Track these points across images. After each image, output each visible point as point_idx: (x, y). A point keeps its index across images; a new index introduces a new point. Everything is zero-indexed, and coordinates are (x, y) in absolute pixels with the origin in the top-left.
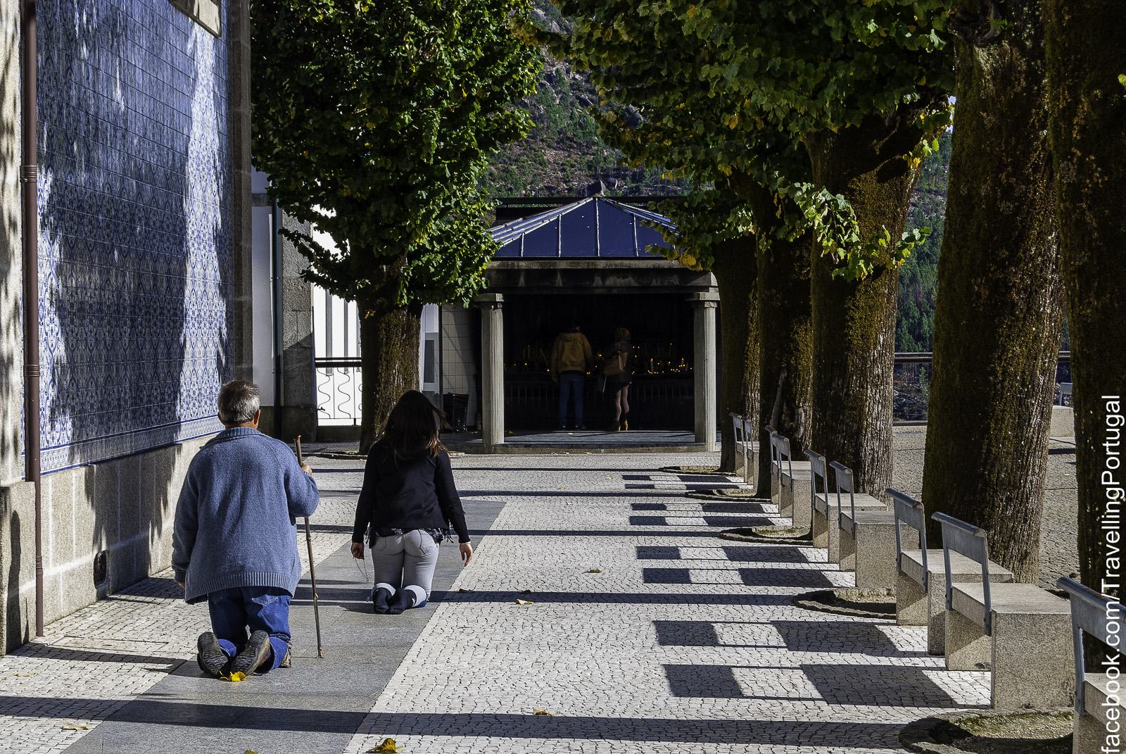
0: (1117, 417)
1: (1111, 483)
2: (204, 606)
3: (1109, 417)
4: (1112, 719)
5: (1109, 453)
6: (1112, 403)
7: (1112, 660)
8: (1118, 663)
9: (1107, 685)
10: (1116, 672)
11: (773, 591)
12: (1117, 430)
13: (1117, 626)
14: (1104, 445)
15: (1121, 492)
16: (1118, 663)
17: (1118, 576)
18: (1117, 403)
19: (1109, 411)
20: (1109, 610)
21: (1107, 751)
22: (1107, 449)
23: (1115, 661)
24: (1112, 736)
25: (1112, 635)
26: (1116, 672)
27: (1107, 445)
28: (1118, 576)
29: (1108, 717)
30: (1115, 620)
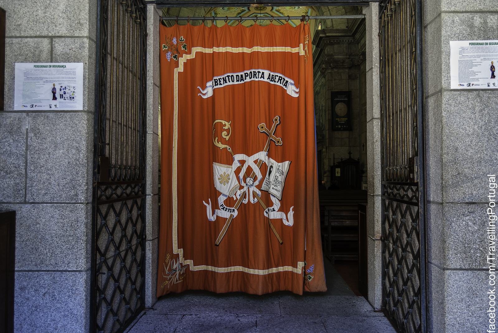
0: (494, 184)
1: (491, 213)
2: (357, 160)
3: (490, 184)
4: (492, 317)
5: (490, 200)
6: (492, 178)
7: (492, 291)
8: (494, 293)
9: (490, 303)
10: (494, 204)
11: (204, 62)
12: (494, 190)
13: (491, 186)
14: (488, 196)
15: (496, 186)
16: (494, 293)
17: (209, 199)
18: (494, 178)
19: (494, 235)
20: (491, 269)
21: (490, 332)
22: (490, 199)
23: (493, 292)
24: (492, 325)
25: (492, 319)
26: (493, 204)
27: (490, 196)
28: (209, 199)
29: (490, 317)
30: (493, 201)
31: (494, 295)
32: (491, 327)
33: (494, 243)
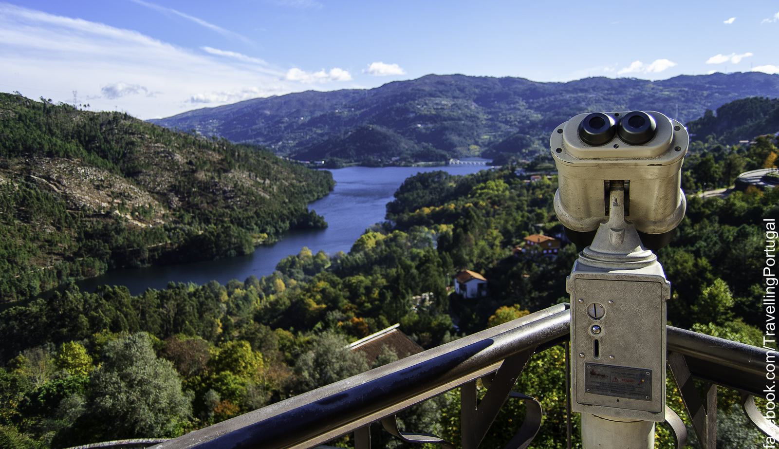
0: (773, 232)
1: (770, 275)
18: (773, 224)
20: (768, 357)
31: (769, 400)
32: (769, 225)
33: (774, 318)
